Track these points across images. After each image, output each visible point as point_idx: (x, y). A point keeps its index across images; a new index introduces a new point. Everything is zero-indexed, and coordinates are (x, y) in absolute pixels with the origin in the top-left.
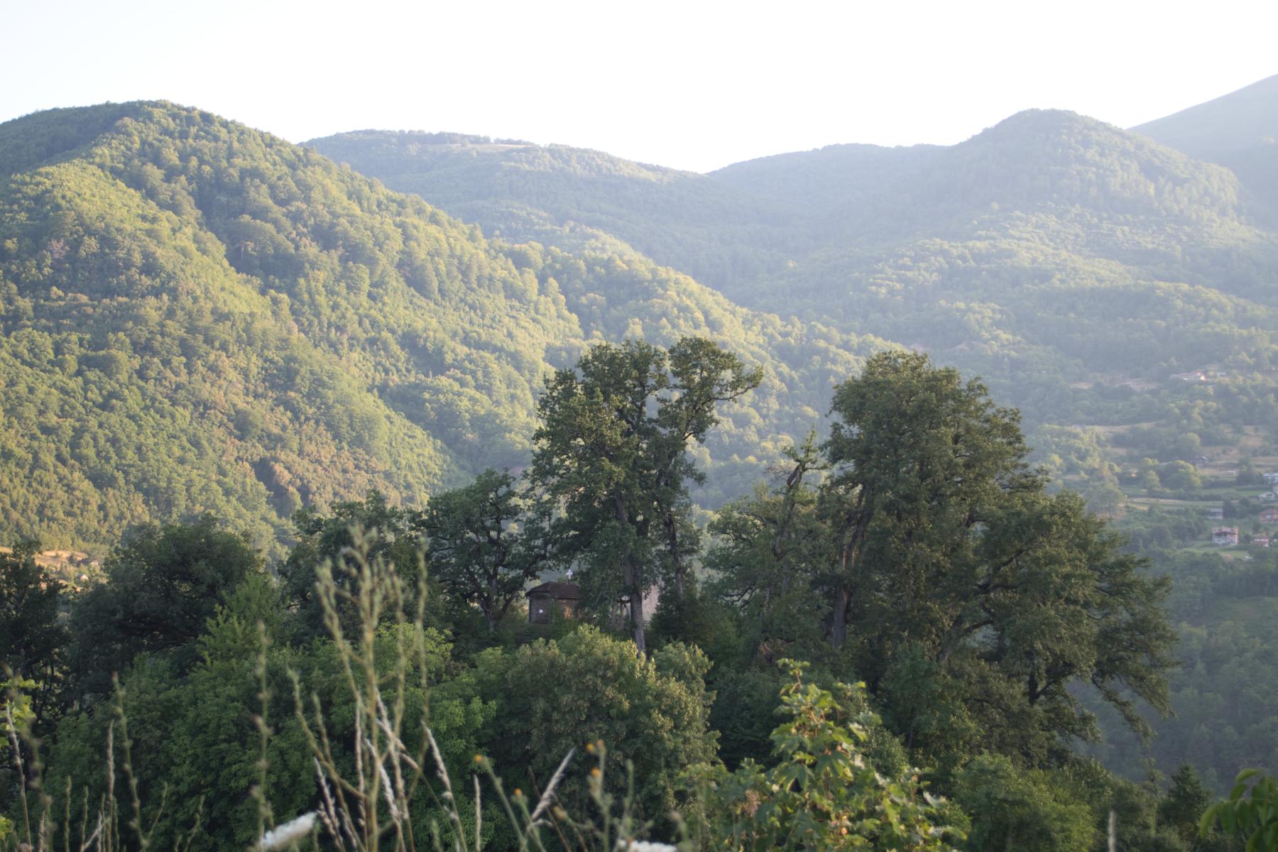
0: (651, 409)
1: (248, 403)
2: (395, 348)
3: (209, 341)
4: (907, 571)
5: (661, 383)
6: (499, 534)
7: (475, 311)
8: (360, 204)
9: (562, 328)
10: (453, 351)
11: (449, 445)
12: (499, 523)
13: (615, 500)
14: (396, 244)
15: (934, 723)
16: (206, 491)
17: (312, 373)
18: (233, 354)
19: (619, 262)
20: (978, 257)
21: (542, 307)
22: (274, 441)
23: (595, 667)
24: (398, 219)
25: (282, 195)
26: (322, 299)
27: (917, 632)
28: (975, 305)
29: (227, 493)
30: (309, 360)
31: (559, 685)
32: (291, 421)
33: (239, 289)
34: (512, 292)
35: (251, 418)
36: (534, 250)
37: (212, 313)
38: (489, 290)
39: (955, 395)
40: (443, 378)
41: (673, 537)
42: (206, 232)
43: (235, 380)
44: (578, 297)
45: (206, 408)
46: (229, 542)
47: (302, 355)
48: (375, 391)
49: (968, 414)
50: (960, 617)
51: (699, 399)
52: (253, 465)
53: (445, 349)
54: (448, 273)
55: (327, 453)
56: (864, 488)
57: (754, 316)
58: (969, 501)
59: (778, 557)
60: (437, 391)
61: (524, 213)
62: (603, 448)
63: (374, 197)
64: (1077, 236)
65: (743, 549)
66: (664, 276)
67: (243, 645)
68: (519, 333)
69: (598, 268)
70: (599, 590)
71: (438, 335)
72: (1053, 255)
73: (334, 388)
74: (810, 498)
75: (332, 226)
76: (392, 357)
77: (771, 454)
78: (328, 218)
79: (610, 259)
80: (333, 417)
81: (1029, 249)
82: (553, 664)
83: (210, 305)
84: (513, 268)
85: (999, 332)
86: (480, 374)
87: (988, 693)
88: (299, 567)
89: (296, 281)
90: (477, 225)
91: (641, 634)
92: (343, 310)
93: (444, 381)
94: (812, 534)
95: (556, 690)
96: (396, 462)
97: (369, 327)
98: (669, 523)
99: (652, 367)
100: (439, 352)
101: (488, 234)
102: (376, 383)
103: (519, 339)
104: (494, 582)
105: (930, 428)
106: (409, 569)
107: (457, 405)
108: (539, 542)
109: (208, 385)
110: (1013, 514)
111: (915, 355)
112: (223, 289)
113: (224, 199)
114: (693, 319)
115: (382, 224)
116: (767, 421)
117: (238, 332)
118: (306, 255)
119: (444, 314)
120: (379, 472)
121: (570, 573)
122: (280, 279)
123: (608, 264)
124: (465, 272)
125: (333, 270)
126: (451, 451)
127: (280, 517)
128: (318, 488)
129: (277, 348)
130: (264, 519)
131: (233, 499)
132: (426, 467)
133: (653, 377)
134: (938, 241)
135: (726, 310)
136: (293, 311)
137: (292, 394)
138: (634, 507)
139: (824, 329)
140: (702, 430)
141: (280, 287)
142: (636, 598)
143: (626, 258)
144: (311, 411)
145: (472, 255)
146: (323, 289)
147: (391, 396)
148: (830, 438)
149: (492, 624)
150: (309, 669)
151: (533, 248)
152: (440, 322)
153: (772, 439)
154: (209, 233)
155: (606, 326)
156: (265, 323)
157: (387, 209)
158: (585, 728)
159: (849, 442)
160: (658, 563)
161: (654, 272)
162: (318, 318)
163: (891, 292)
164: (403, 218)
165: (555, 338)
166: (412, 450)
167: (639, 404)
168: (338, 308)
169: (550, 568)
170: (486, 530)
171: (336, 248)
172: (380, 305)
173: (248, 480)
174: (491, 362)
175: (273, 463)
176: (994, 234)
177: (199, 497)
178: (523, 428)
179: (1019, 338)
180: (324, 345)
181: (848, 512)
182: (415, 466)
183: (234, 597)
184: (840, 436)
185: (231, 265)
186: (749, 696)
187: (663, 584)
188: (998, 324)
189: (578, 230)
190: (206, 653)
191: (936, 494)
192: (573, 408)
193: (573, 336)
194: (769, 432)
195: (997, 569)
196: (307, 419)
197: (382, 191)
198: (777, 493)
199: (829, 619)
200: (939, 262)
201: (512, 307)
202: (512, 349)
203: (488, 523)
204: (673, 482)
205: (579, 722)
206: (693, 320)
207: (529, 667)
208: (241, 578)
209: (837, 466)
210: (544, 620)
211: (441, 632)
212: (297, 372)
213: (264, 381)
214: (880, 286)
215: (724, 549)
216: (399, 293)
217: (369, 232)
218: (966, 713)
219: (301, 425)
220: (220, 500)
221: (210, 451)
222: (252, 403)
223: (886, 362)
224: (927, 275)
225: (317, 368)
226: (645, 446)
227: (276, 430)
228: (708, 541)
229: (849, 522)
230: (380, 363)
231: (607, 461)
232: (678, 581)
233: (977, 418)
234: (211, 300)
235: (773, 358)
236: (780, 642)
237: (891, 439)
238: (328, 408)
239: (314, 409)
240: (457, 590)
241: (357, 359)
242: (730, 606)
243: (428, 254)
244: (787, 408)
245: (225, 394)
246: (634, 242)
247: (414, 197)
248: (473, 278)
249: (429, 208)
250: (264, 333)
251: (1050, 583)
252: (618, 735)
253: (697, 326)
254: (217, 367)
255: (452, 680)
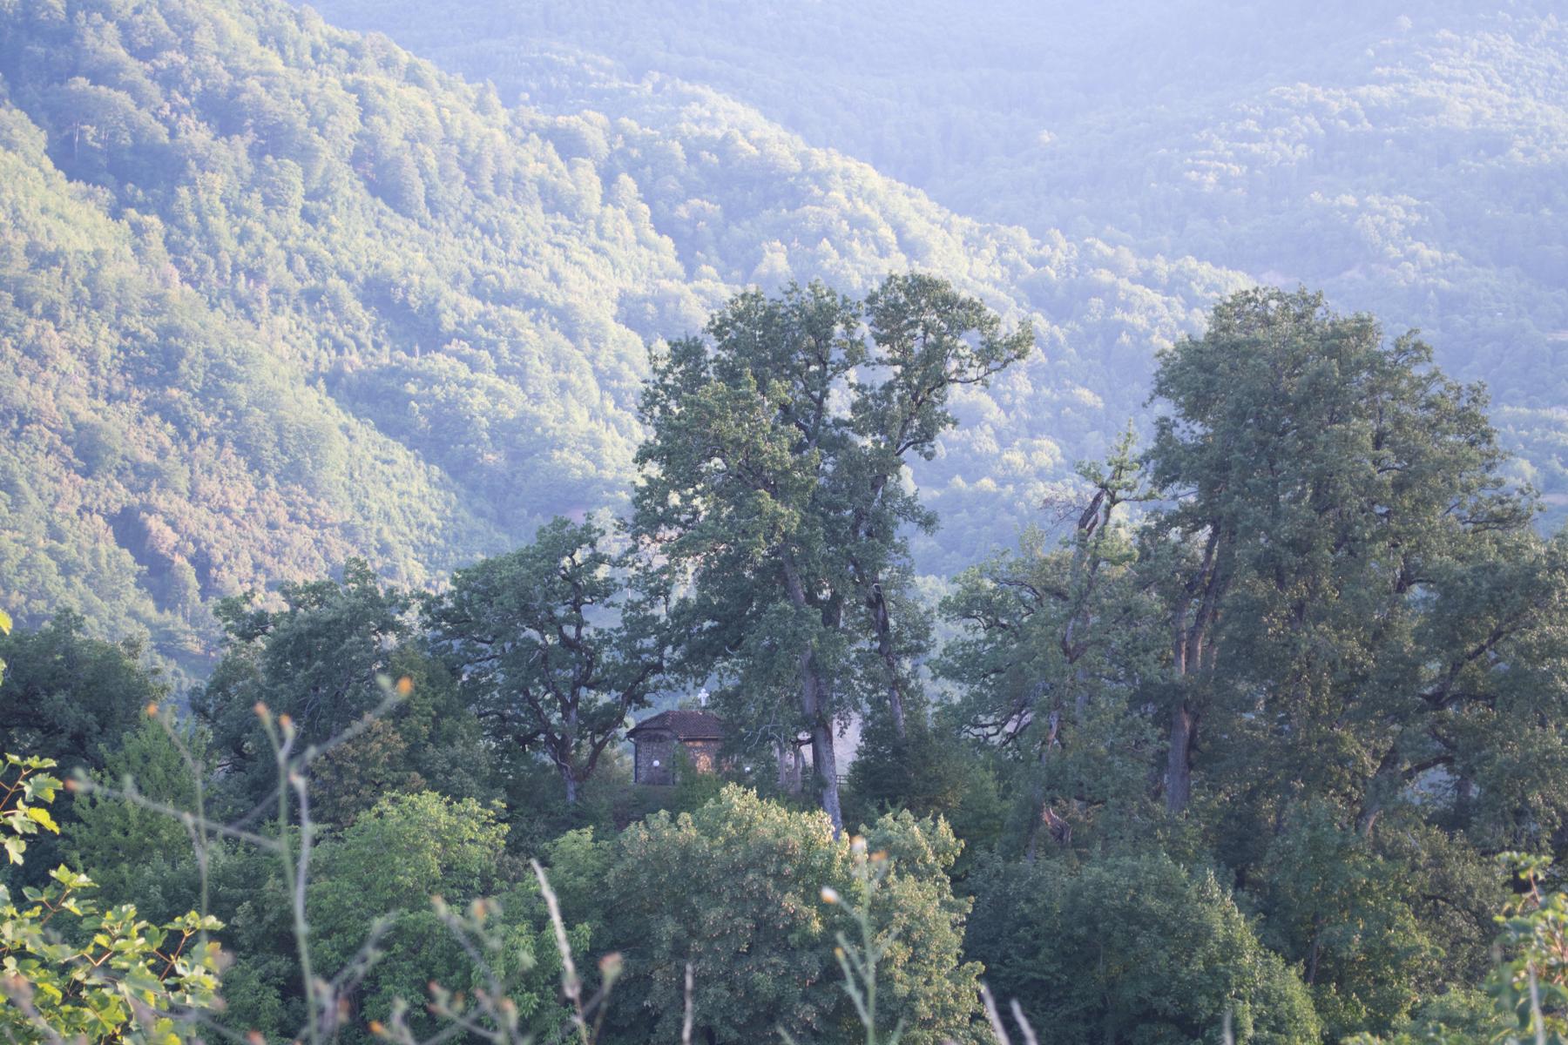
0: (839, 402)
1: (96, 411)
2: (353, 306)
3: (23, 303)
4: (1297, 676)
5: (855, 355)
6: (579, 628)
7: (492, 237)
8: (282, 51)
9: (645, 261)
10: (455, 308)
11: (454, 475)
12: (578, 610)
13: (782, 565)
14: (348, 122)
15: (1357, 938)
16: (29, 568)
17: (208, 354)
18: (68, 324)
19: (743, 143)
20: (1377, 114)
21: (609, 228)
22: (145, 476)
23: (762, 858)
24: (349, 77)
25: (143, 41)
26: (220, 224)
27: (1319, 779)
28: (1374, 200)
29: (66, 569)
30: (202, 332)
31: (699, 892)
32: (174, 440)
33: (72, 209)
34: (554, 201)
35: (102, 437)
36: (592, 126)
37: (28, 253)
38: (516, 199)
39: (1374, 363)
40: (439, 357)
41: (885, 626)
42: (10, 110)
43: (71, 369)
44: (671, 208)
45: (23, 421)
46: (105, 658)
47: (189, 323)
48: (321, 383)
49: (1397, 395)
50: (1393, 751)
51: (923, 383)
52: (111, 519)
53: (441, 305)
54: (442, 171)
55: (240, 494)
56: (1216, 531)
57: (983, 231)
58: (1404, 547)
59: (1072, 654)
60: (429, 380)
61: (572, 59)
62: (758, 475)
63: (306, 39)
64: (1552, 71)
65: (1003, 643)
66: (823, 164)
67: (140, 839)
68: (571, 274)
69: (705, 154)
70: (759, 722)
71: (427, 282)
72: (1510, 106)
73: (249, 381)
74: (1125, 551)
75: (235, 92)
76: (349, 322)
77: (1020, 474)
78: (226, 78)
79: (726, 138)
80: (248, 430)
81: (1466, 97)
82: (686, 855)
83: (22, 240)
84: (556, 158)
85: (1418, 246)
86: (504, 349)
87: (1445, 884)
88: (228, 698)
89: (173, 192)
90: (490, 84)
91: (833, 797)
92: (259, 242)
93: (440, 362)
94: (1129, 613)
95: (694, 900)
96: (361, 508)
97: (306, 271)
98: (876, 602)
99: (839, 328)
100: (432, 311)
101: (509, 99)
102: (322, 369)
103: (571, 284)
104: (573, 715)
105: (1332, 421)
106: (425, 697)
107: (466, 404)
108: (650, 642)
109: (25, 381)
110: (1485, 569)
111: (1302, 293)
112: (44, 211)
113: (40, 51)
114: (876, 240)
115: (321, 87)
116: (1012, 415)
117: (74, 286)
118: (190, 145)
119: (438, 243)
120: (332, 525)
121: (703, 695)
122: (145, 189)
123: (723, 147)
124: (471, 169)
125: (238, 171)
126: (457, 485)
127: (160, 610)
128: (226, 557)
129: (145, 312)
130: (133, 614)
131: (77, 581)
132: (415, 514)
133: (841, 346)
134: (1305, 87)
135: (933, 222)
136: (171, 247)
137: (175, 393)
138: (816, 575)
139: (1108, 251)
140: (929, 437)
141: (146, 203)
142: (821, 736)
143: (755, 135)
144: (208, 422)
145: (483, 138)
146: (222, 206)
147: (348, 390)
148: (1152, 445)
149: (571, 788)
150: (257, 876)
151: (590, 123)
152: (430, 259)
153: (1023, 448)
154: (16, 112)
155: (724, 256)
156: (122, 269)
157: (330, 60)
158: (751, 964)
159: (1189, 450)
160: (859, 673)
161: (805, 158)
162: (215, 257)
163: (1225, 181)
164: (358, 76)
165: (634, 280)
166: (388, 484)
167: (817, 394)
168: (249, 238)
169: (669, 686)
170: (556, 624)
171: (241, 131)
172: (323, 230)
173: (102, 547)
174: (522, 326)
175: (144, 515)
176: (1404, 72)
177: (17, 579)
178: (584, 440)
179: (1453, 255)
180: (228, 304)
181: (1187, 573)
182: (395, 513)
183: (120, 754)
184: (1170, 440)
185: (57, 167)
186: (1029, 900)
187: (867, 709)
188: (1415, 232)
189: (668, 87)
190: (76, 854)
191: (1345, 539)
192: (706, 406)
193: (665, 276)
194: (1017, 434)
195: (1457, 666)
196: (203, 436)
197: (320, 28)
198: (1066, 544)
199: (1162, 759)
200: (1308, 126)
201: (556, 228)
202: (560, 302)
203: (561, 612)
204: (881, 530)
205: (737, 956)
206: (877, 244)
207: (645, 861)
208: (133, 721)
209: (1169, 491)
210: (662, 779)
211: (486, 805)
212: (181, 354)
213: (123, 370)
214: (1205, 170)
215: (969, 644)
216: (357, 207)
217: (299, 102)
218: (1411, 922)
219: (191, 446)
220: (55, 582)
221: (33, 498)
222: (103, 411)
223: (1248, 308)
224: (1289, 150)
225: (216, 346)
226: (829, 468)
227: (148, 458)
228: (947, 633)
229: (1191, 591)
230: (326, 334)
231: (768, 495)
232: (894, 703)
233: (1413, 401)
234: (24, 229)
235: (1019, 305)
236: (1076, 804)
237: (1263, 444)
238: (239, 415)
239: (214, 419)
240: (507, 731)
241: (286, 327)
242: (981, 744)
243: (406, 138)
244: (1046, 392)
245: (56, 396)
246: (767, 107)
247: (376, 37)
248: (487, 178)
249: (404, 57)
250: (121, 285)
251: (1552, 692)
252: (804, 975)
253: (883, 252)
254: (40, 348)
255: (511, 888)
